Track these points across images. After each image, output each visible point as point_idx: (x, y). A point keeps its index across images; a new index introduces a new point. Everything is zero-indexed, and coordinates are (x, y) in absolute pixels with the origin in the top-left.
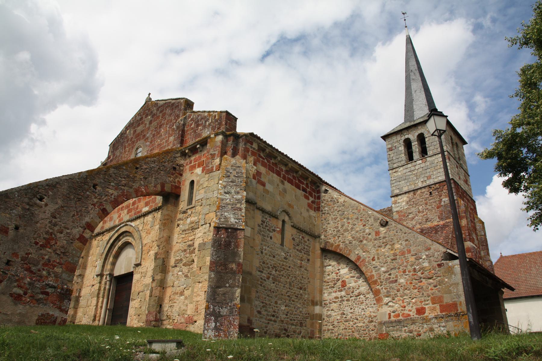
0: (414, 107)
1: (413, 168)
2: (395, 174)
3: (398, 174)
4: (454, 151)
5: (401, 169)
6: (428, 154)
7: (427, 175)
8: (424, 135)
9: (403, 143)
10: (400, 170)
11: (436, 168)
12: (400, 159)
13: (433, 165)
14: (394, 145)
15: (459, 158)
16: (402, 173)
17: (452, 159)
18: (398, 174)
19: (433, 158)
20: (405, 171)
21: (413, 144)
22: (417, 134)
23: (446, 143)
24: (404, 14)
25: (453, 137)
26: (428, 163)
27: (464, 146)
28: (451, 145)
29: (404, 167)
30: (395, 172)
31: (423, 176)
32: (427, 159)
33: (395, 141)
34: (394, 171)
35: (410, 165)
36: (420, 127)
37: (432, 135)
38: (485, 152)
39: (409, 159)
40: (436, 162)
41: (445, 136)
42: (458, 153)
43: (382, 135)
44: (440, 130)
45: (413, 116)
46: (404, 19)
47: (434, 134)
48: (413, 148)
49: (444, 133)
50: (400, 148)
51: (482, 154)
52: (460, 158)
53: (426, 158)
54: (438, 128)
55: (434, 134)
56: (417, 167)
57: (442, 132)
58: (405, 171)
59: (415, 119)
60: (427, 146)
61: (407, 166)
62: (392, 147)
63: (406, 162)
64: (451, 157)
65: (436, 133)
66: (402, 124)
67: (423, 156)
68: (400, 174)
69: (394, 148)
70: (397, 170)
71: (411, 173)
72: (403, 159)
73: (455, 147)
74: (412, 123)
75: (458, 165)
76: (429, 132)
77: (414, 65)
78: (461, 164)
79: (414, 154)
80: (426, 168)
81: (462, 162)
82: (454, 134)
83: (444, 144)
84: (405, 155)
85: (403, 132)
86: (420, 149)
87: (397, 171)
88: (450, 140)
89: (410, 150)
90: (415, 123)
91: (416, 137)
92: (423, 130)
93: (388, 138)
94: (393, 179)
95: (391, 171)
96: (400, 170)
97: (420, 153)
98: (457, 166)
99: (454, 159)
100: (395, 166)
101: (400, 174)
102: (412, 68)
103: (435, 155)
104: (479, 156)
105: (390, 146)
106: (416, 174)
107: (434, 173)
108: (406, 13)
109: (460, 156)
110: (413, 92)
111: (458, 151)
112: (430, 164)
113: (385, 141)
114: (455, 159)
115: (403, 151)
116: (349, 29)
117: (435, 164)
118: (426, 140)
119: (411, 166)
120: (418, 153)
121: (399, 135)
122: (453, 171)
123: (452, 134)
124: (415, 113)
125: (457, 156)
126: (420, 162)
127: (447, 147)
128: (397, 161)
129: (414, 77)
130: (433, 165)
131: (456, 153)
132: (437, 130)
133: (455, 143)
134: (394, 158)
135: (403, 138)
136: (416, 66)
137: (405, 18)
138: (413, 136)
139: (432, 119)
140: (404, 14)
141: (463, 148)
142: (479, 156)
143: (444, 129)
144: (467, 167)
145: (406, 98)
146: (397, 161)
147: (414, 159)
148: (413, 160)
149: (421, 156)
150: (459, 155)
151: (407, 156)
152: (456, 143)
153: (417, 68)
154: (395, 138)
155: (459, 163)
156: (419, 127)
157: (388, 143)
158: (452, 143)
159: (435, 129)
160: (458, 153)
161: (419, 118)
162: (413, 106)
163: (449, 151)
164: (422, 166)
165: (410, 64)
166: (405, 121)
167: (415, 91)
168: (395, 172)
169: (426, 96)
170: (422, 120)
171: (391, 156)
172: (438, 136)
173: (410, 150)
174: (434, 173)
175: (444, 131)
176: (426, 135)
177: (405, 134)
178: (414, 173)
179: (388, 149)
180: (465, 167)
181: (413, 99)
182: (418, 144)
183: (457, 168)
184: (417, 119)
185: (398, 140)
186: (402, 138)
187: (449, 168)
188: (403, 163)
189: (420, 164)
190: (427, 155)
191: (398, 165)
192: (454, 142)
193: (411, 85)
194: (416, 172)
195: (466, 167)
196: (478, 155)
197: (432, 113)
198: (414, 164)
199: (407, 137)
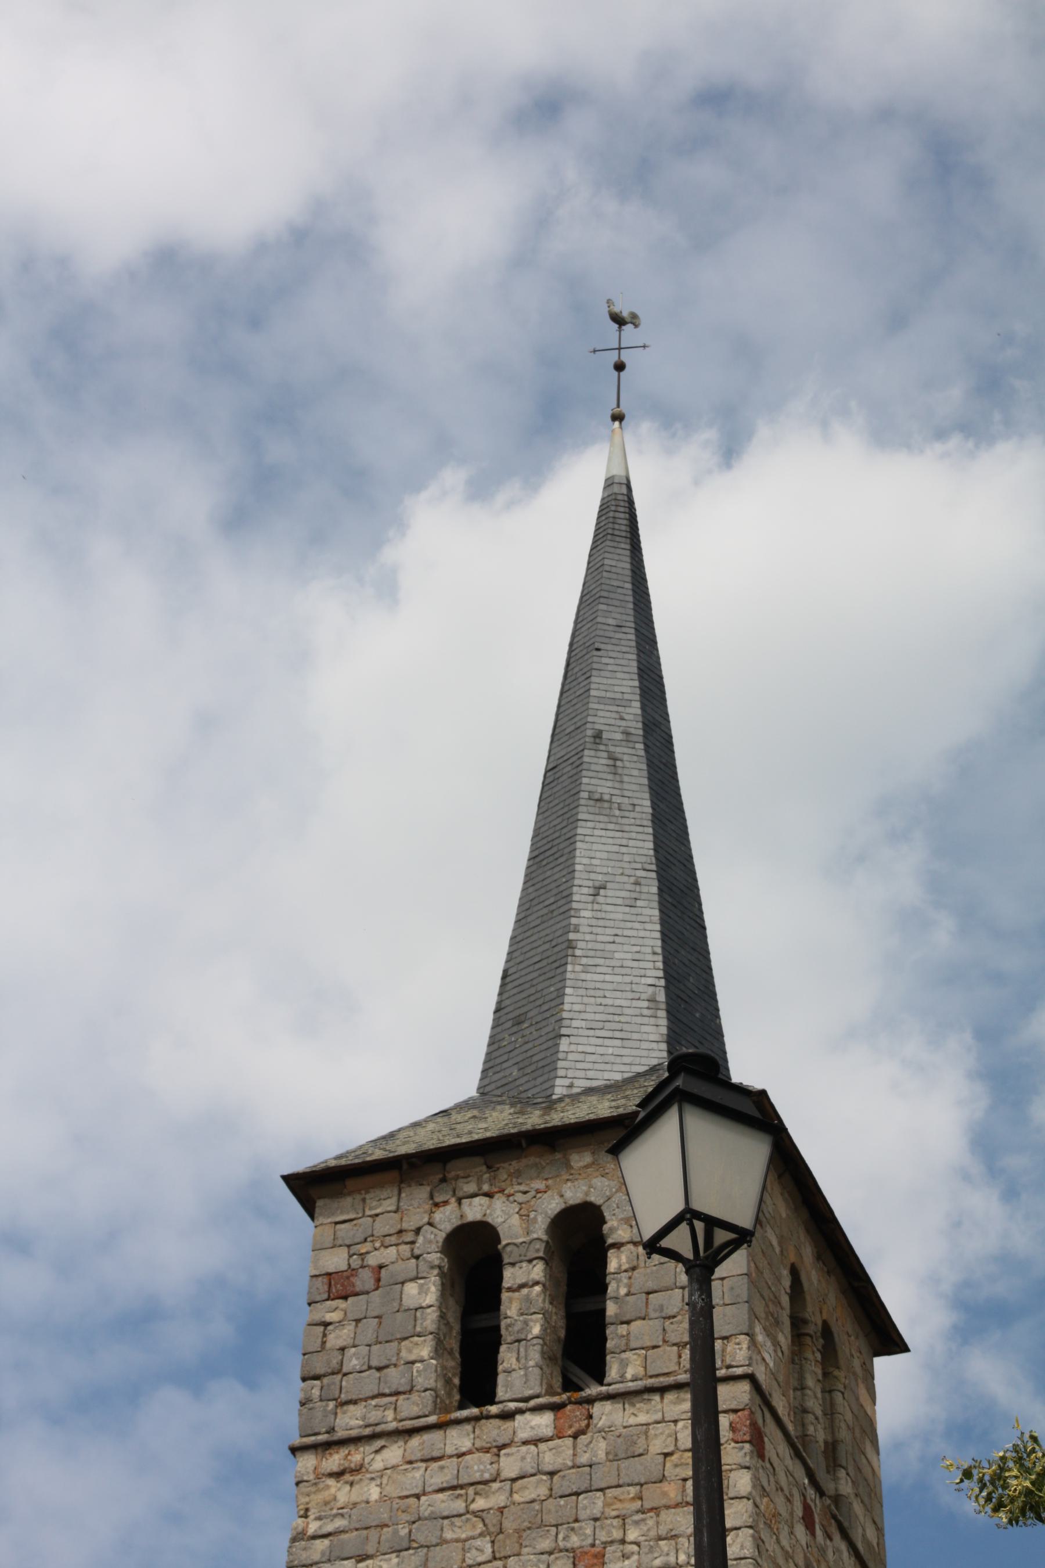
0: (571, 999)
1: (478, 1466)
2: (341, 1492)
3: (356, 1494)
4: (802, 1388)
5: (394, 1453)
6: (613, 1372)
7: (575, 1541)
8: (603, 1221)
9: (435, 1258)
10: (378, 1463)
11: (653, 1496)
12: (395, 1378)
13: (633, 1470)
14: (372, 1260)
15: (832, 1448)
16: (392, 1491)
17: (776, 1447)
18: (356, 1494)
19: (641, 1414)
20: (415, 1478)
21: (510, 1276)
22: (552, 1205)
23: (753, 1315)
24: (619, 320)
25: (813, 1277)
26: (601, 1448)
27: (882, 1364)
28: (784, 1339)
29: (415, 1441)
30: (338, 1475)
31: (546, 1544)
32: (597, 1409)
33: (385, 1225)
34: (334, 1461)
35: (459, 1439)
36: (587, 1158)
37: (653, 1246)
38: (1019, 1461)
39: (463, 1389)
40: (658, 1445)
41: (751, 1258)
42: (830, 1412)
43: (285, 1173)
44: (712, 1223)
45: (548, 1067)
46: (613, 357)
47: (665, 1243)
48: (511, 1307)
49: (733, 1246)
50: (411, 1289)
51: (999, 1478)
52: (842, 1451)
53: (591, 1401)
54: (696, 1206)
55: (665, 1243)
56: (510, 1464)
57: (721, 1237)
58: (415, 1478)
59: (559, 1091)
60: (611, 1309)
61: (436, 1436)
62: (352, 1271)
63: (440, 1407)
64: (770, 1429)
65: (680, 1240)
66: (460, 1107)
67: (569, 1385)
68: (374, 1493)
69: (364, 1280)
70: (356, 1455)
71: (459, 1506)
72: (421, 1382)
73: (813, 1355)
74: (534, 1120)
75: (817, 1506)
76: (632, 1220)
77: (626, 704)
78: (837, 1499)
79: (507, 1357)
80: (573, 1481)
81: (846, 1488)
82: (819, 1257)
83: (724, 1320)
84: (440, 1349)
85: (456, 1168)
86: (560, 1322)
87: (358, 1469)
88: (785, 1300)
89: (482, 1321)
90: (557, 1118)
91: (540, 1230)
92: (598, 1182)
93: (339, 1194)
94: (313, 1527)
95: (308, 1462)
96: (378, 1463)
97: (548, 1357)
98: (807, 1508)
99: (798, 1449)
100: (350, 1421)
101: (374, 1493)
102: (602, 717)
103: (662, 1390)
104: (972, 1485)
105: (336, 1261)
106: (492, 1519)
107: (632, 1535)
108: (634, 320)
109: (843, 1434)
110: (580, 895)
111: (828, 1391)
112: (613, 1457)
113: (312, 1215)
114: (797, 1455)
115: (430, 1320)
116: (255, 322)
117: (651, 1464)
118: (612, 1265)
119: (466, 1444)
120: (535, 1356)
121: (423, 1192)
122: (770, 1544)
123: (808, 1252)
124: (564, 1045)
125: (819, 1433)
126: (543, 1423)
127: (753, 1343)
128: (369, 1383)
129: (605, 788)
130: (633, 1470)
131: (815, 1404)
132: (688, 1215)
133: (814, 1327)
134: (353, 1361)
135: (447, 1218)
136: (636, 708)
137: (626, 357)
138: (524, 1217)
139: (668, 1126)
140: (619, 320)
141: (869, 1375)
142: (972, 1485)
143: (745, 1221)
144: (880, 1530)
145: (521, 921)
146: (369, 1383)
147: (501, 1393)
148: (490, 1398)
149: (557, 1382)
150: (832, 1427)
151: (453, 1364)
152: (827, 1331)
153: (636, 727)
154: (389, 1205)
155: (829, 1487)
156: (580, 1159)
157: (329, 1231)
158: (798, 1323)
159: (679, 1207)
160: (830, 1412)
161: (589, 1091)
162: (561, 995)
163: (761, 1377)
164: (552, 1456)
165: (600, 685)
166: (482, 1090)
167: (598, 890)
168: (338, 1475)
169: (666, 936)
170: (603, 1108)
171: (337, 1338)
172: (690, 1267)
173: (482, 1321)
174: (632, 1535)
175: (742, 1237)
176: (616, 1229)
177: (471, 1187)
178: (480, 1504)
179: (321, 1284)
180: (863, 1532)
181: (571, 945)
182: (550, 1284)
183: (810, 1526)
184: (575, 1098)
185: (410, 1224)
186: (438, 1216)
187: (735, 1514)
188: (412, 1407)
189: (536, 1442)
190: (599, 1377)
191: (374, 1416)
192: (814, 1313)
193: (571, 840)
194: (500, 1499)
195: (871, 1534)
196: (967, 1474)
197: (679, 1082)
198: (493, 1431)
199: (474, 1210)
